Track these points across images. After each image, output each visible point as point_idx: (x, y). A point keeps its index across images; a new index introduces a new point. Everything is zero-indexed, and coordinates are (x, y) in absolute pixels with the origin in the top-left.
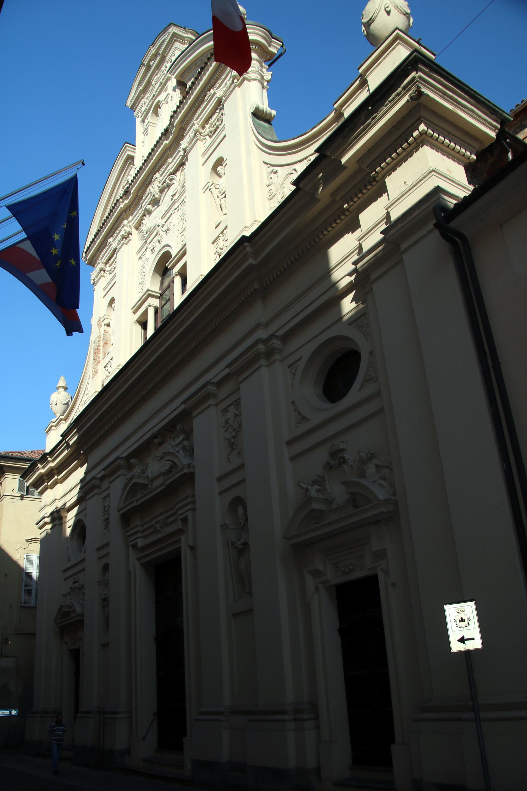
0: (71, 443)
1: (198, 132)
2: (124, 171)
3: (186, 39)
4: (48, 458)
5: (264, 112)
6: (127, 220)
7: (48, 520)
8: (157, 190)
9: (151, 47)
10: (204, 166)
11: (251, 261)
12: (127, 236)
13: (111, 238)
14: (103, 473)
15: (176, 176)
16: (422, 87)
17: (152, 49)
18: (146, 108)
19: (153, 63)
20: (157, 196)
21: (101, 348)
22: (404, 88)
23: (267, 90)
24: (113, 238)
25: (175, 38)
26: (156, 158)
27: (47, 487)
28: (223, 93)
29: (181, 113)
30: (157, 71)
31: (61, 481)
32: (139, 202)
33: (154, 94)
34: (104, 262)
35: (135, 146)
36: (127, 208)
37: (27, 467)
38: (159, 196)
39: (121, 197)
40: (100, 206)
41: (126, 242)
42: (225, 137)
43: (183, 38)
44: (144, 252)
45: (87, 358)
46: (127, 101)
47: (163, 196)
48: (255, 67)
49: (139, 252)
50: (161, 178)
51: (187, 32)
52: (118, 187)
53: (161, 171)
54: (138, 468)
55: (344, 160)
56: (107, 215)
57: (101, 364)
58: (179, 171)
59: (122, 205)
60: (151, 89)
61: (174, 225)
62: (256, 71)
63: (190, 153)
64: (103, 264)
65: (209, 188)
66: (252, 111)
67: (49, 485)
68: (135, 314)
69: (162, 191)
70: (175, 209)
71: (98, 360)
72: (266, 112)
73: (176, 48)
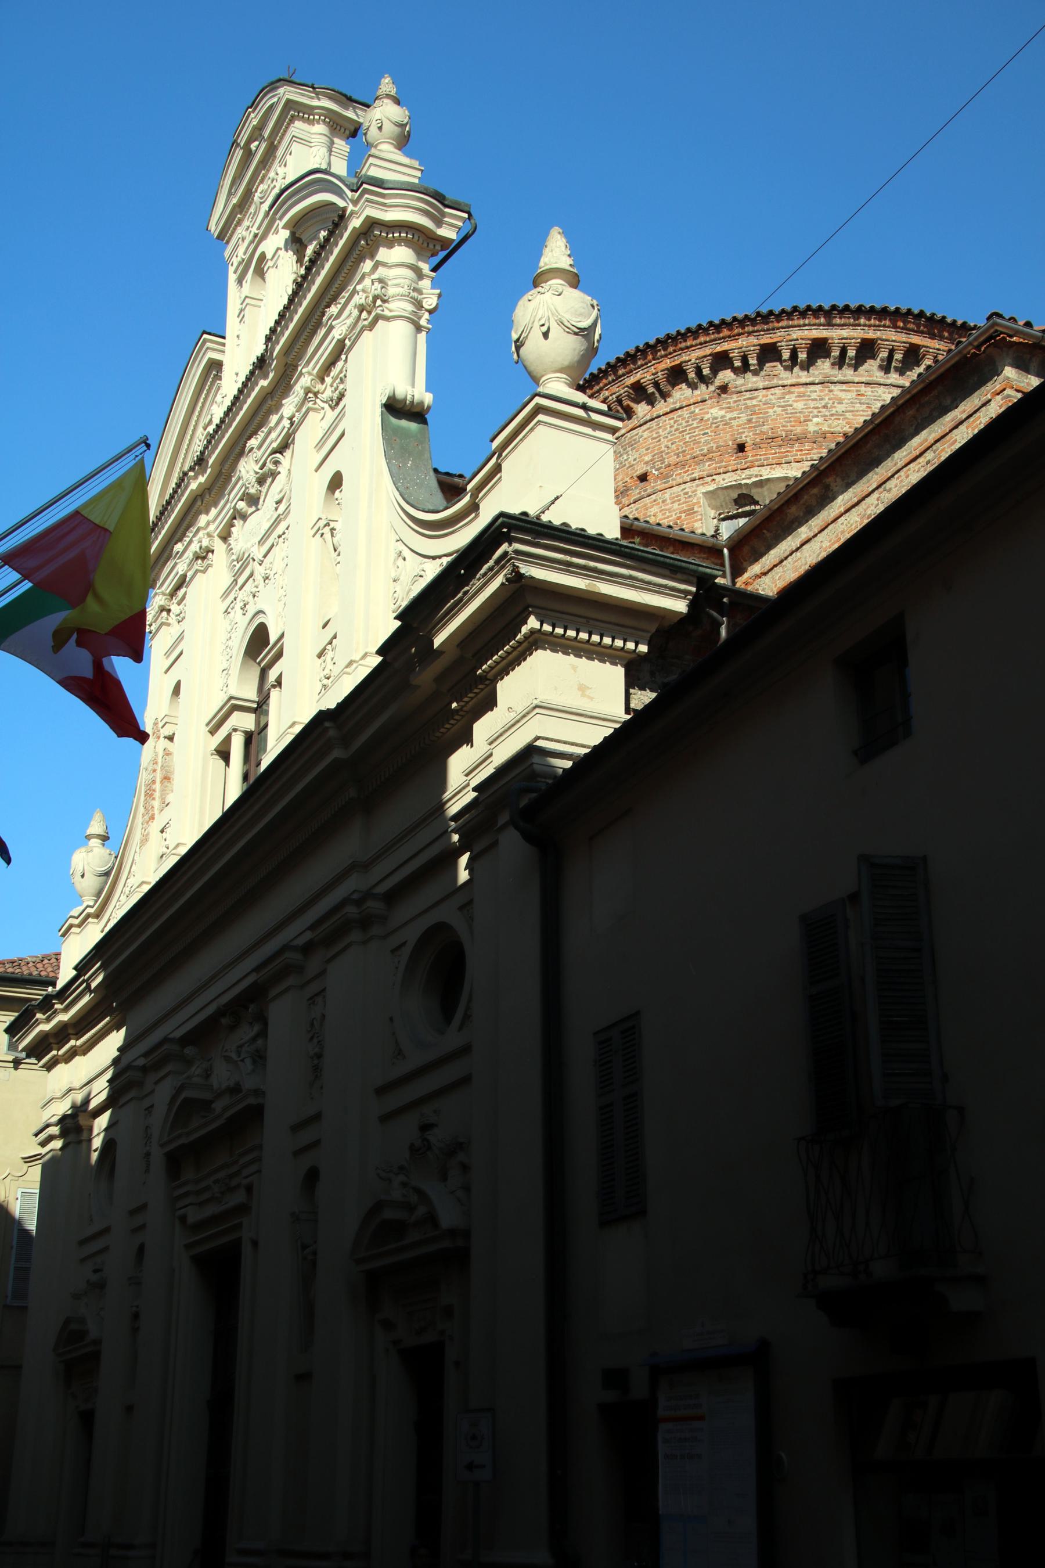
0: (94, 985)
1: (310, 392)
2: (205, 392)
3: (316, 111)
4: (54, 1004)
5: (408, 402)
6: (372, 261)
7: (55, 1130)
8: (252, 478)
9: (250, 110)
10: (318, 472)
11: (337, 753)
12: (205, 554)
13: (179, 543)
14: (308, 936)
15: (284, 457)
16: (520, 566)
17: (253, 115)
18: (244, 257)
19: (257, 147)
20: (252, 491)
21: (157, 786)
22: (497, 562)
23: (427, 332)
24: (183, 545)
25: (292, 112)
26: (233, 431)
27: (57, 1060)
28: (347, 331)
29: (283, 336)
30: (263, 172)
31: (84, 1051)
32: (223, 488)
33: (257, 232)
34: (168, 591)
35: (224, 338)
36: (204, 490)
37: (41, 997)
38: (257, 491)
39: (192, 469)
40: (160, 458)
41: (202, 569)
42: (343, 435)
43: (310, 110)
44: (232, 602)
45: (135, 797)
46: (210, 220)
47: (264, 489)
48: (402, 285)
49: (226, 597)
50: (260, 453)
51: (317, 94)
52: (194, 423)
53: (263, 432)
54: (198, 1067)
55: (438, 641)
56: (167, 497)
57: (155, 821)
58: (289, 449)
59: (194, 486)
60: (252, 210)
61: (276, 573)
62: (405, 296)
63: (298, 431)
64: (164, 597)
65: (320, 532)
66: (384, 402)
67: (60, 1056)
68: (213, 736)
69: (261, 481)
70: (279, 537)
71: (151, 813)
72: (412, 402)
73: (294, 138)
